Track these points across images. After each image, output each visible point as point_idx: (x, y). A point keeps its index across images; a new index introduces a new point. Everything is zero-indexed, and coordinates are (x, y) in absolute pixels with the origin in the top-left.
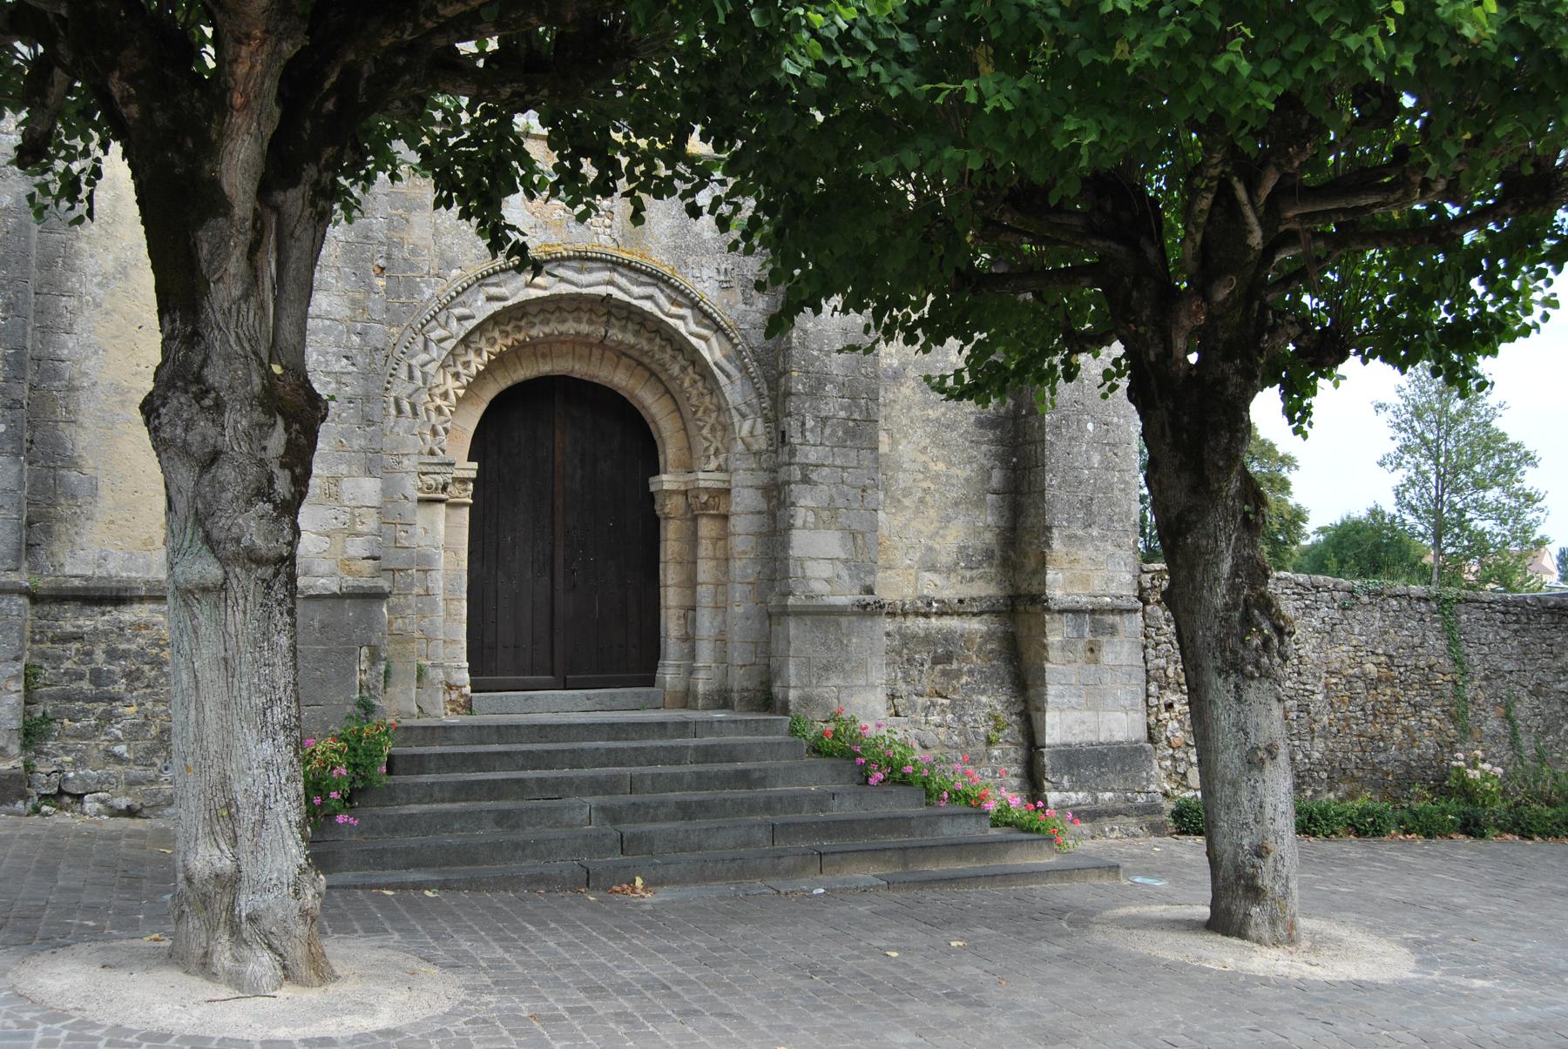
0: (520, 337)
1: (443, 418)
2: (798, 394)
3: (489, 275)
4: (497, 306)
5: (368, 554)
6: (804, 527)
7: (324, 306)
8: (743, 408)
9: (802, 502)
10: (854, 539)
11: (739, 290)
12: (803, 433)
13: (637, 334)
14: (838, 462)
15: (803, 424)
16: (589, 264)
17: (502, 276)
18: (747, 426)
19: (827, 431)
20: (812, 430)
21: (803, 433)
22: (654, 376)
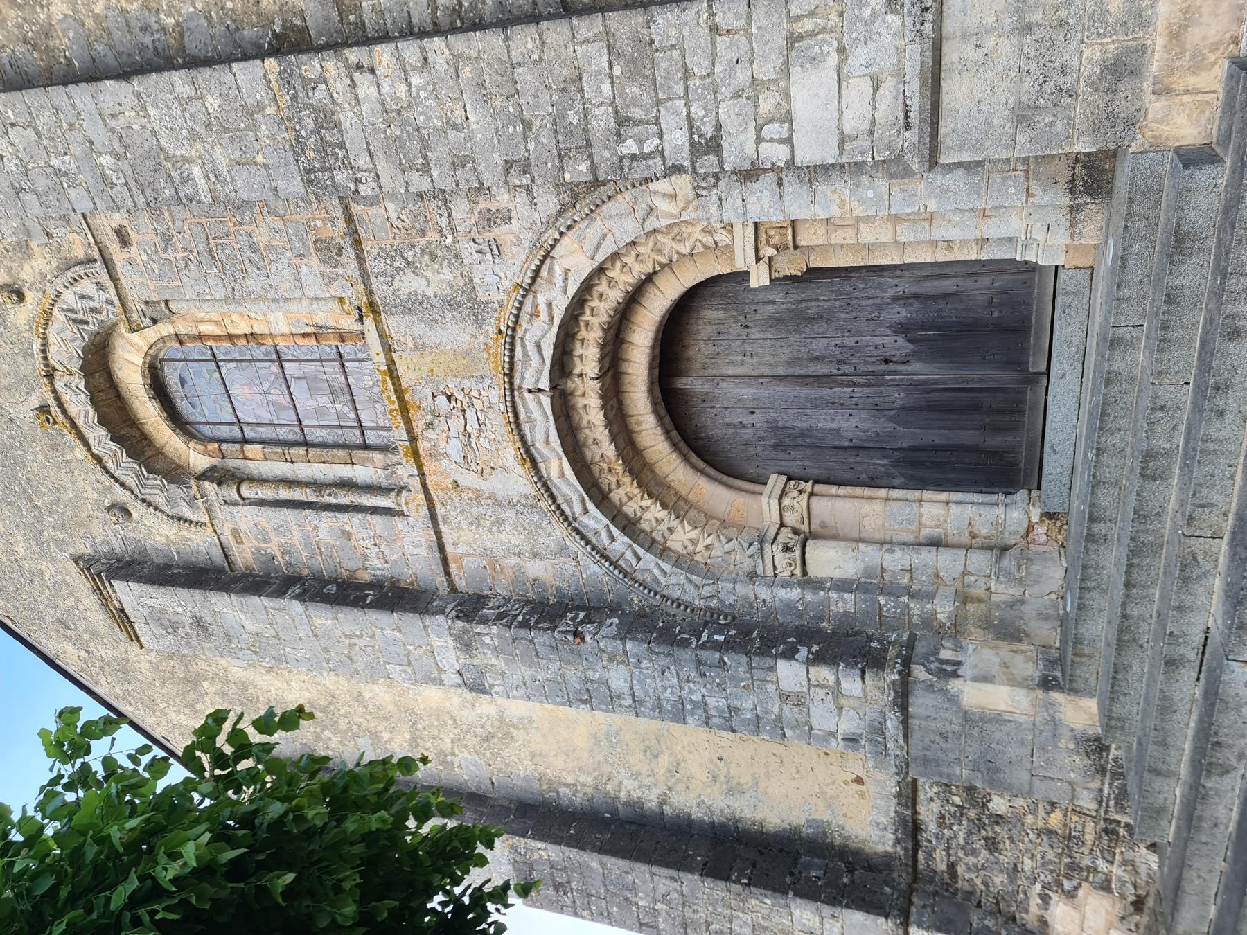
0: (620, 469)
1: (717, 544)
2: (593, 168)
3: (563, 513)
4: (591, 506)
5: (859, 680)
6: (789, 141)
7: (621, 683)
8: (640, 214)
9: (750, 149)
10: (800, 37)
11: (497, 231)
12: (646, 157)
13: (507, 662)
14: (679, 89)
15: (633, 157)
16: (522, 416)
17: (560, 500)
18: (663, 205)
19: (637, 114)
20: (640, 142)
21: (646, 157)
22: (634, 298)
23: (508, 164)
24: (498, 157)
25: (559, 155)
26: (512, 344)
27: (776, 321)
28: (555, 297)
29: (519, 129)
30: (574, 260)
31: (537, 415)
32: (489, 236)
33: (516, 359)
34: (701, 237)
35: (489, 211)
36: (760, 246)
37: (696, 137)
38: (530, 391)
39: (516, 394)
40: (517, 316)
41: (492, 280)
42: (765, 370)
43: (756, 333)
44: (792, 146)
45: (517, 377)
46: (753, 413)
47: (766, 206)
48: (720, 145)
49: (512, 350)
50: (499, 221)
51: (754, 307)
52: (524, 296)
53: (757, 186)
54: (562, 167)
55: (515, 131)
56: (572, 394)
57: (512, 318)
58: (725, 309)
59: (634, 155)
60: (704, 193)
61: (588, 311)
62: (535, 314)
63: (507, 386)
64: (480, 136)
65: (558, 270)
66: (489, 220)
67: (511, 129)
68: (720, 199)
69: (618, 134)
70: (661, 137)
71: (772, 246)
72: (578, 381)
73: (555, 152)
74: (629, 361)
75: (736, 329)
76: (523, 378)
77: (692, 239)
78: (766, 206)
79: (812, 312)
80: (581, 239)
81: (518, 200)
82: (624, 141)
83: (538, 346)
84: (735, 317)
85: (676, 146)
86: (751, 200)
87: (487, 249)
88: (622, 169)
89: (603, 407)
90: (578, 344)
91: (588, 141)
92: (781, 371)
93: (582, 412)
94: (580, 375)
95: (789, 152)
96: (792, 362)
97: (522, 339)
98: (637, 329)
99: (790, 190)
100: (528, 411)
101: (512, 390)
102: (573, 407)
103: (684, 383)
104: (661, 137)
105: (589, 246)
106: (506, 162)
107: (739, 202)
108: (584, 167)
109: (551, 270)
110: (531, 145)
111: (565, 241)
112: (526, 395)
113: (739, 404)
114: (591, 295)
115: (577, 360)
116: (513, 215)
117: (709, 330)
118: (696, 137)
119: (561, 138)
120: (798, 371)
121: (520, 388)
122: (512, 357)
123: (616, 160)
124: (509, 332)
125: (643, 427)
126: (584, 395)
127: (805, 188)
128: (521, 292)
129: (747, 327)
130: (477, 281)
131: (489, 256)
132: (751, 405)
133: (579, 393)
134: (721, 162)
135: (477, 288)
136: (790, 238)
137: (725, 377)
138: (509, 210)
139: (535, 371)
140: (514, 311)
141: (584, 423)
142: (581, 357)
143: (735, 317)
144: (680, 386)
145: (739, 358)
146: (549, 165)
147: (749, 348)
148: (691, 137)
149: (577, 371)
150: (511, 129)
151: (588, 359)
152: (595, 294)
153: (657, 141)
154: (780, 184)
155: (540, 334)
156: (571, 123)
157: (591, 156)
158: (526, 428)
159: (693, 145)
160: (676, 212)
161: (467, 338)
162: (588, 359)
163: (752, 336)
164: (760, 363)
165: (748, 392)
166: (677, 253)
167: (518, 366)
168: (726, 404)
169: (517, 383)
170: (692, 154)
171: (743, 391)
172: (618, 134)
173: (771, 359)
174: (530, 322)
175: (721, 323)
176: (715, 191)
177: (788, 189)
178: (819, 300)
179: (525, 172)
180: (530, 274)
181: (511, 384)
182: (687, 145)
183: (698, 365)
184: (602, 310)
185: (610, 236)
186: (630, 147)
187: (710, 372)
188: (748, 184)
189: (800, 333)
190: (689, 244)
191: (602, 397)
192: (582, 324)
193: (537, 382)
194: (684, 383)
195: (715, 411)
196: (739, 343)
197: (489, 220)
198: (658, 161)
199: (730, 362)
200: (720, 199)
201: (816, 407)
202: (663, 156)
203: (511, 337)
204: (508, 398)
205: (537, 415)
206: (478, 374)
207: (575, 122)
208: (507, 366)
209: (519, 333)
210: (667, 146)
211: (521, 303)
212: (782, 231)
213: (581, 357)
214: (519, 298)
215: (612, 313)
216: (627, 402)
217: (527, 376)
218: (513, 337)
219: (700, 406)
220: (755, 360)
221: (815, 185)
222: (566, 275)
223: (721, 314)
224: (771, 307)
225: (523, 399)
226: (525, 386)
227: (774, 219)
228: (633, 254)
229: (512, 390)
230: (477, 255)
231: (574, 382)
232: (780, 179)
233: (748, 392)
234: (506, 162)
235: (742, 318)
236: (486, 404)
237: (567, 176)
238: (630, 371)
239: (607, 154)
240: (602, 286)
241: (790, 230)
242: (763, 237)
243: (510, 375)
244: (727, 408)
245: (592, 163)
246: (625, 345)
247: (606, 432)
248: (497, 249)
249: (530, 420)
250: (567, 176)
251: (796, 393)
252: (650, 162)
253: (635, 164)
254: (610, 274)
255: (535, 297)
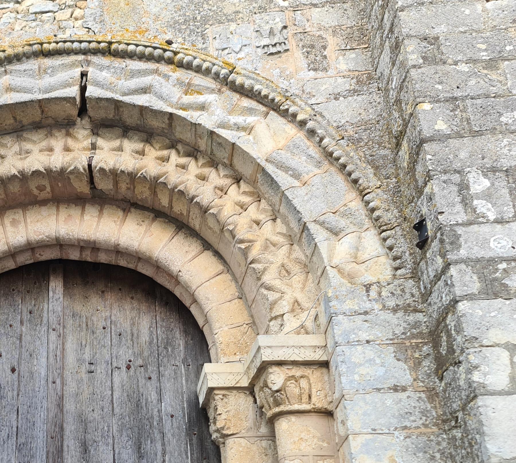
8: (331, 218)
12: (466, 202)
15: (463, 187)
16: (48, 62)
21: (466, 202)
23: (434, 41)
24: (441, 30)
25: (456, 99)
26: (150, 58)
27: (137, 404)
28: (216, 113)
29: (484, 56)
30: (265, 139)
31: (48, 81)
32: (292, 44)
33: (128, 61)
34: (288, 298)
35: (324, 48)
36: (284, 368)
37: (504, 265)
38: (84, 75)
39: (81, 57)
40: (188, 66)
41: (236, 43)
42: (71, 387)
43: (120, 378)
44: (508, 393)
45: (105, 61)
46: (13, 370)
47: (363, 370)
48: (496, 296)
49: (142, 57)
50: (312, 57)
51: (154, 376)
52: (217, 75)
53: (390, 359)
54: (438, 101)
55: (480, 50)
56: (68, 134)
57: (187, 59)
58: (151, 343)
59: (468, 187)
60: (373, 294)
61: (183, 160)
62: (189, 89)
63: (93, 45)
64: (467, 12)
65: (251, 119)
66: (312, 47)
67: (483, 47)
68: (366, 313)
69: (494, 170)
70: (497, 221)
71: (284, 384)
72: (87, 143)
73: (458, 93)
74: (101, 211)
75: (125, 354)
76: (102, 68)
77: (284, 288)
78: (363, 370)
79: (147, 446)
80: (292, 148)
81: (340, 80)
82: (485, 175)
83: (145, 90)
84: (141, 354)
85: (486, 241)
86: (369, 352)
87: (276, 40)
88: (445, 172)
89: (49, 171)
90: (139, 146)
91: (479, 133)
92: (70, 406)
93: (44, 144)
94: (94, 147)
95: (499, 388)
96: (83, 421)
97: (156, 71)
98: (142, 229)
99: (389, 402)
100: (54, 70)
101: (85, 52)
102: (50, 134)
103: (56, 287)
104: (497, 221)
105: (285, 157)
106: (437, 38)
107: (365, 336)
108: (441, 126)
109: (250, 111)
110: (464, 67)
111: (291, 130)
112: (77, 72)
113: (25, 355)
114: (204, 165)
115: (117, 143)
116: (320, 74)
117: (124, 323)
118: (503, 266)
119: (479, 101)
120: (70, 428)
121: (89, 63)
122: (131, 56)
123: (457, 165)
124: (168, 54)
125: (9, 229)
126: (67, 149)
127: (394, 421)
128: (224, 72)
129: (128, 367)
130: (233, 26)
131: (266, 41)
132: (24, 368)
133: (70, 142)
134: (470, 297)
135: (222, 26)
136: (296, 407)
137: (62, 337)
138: (325, 70)
139: (108, 81)
140: (196, 63)
141: (28, 146)
142: (120, 149)
143: (141, 354)
144: (52, 284)
145: (87, 357)
146: (440, 87)
147: (101, 369)
148: (503, 260)
149: (100, 142)
150: (483, 47)
151: (117, 155)
152: (206, 171)
153: (492, 217)
154: (395, 389)
155: (163, 92)
156: (501, 115)
157: (459, 136)
158: (32, 64)
159: (492, 261)
160: (336, 261)
161: (155, 10)
162: (117, 155)
163: (116, 373)
164: (80, 382)
165: (41, 366)
166: (265, 269)
167: (118, 63)
168: (26, 338)
169: (95, 59)
170: (478, 260)
171: (44, 360)
172: (494, 170)
173: (86, 394)
174: (180, 83)
175: (134, 337)
176: (377, 306)
177: (390, 399)
178: (164, 454)
179: (424, 58)
180: (247, 83)
181: (95, 52)
182: (489, 255)
183: (78, 307)
184: (184, 178)
185: (296, 183)
186: (479, 184)
187: (70, 322)
188: (392, 349)
189: (121, 431)
190: (277, 283)
191: (62, 171)
192: (165, 152)
193: (97, 84)
194: (56, 287)
195: (16, 324)
196: (108, 357)
197: (312, 47)
198: (462, 217)
199: (82, 347)
200: (366, 313)
201: (19, 449)
202: (470, 223)
203: (161, 57)
204: (76, 45)
205: (48, 81)
206: (107, 18)
207: (503, 119)
208: (122, 47)
209: (164, 68)
210: (485, 229)
211: (207, 72)
212: (305, 398)
213: (120, 149)
214: (215, 69)
215: (181, 187)
216: (44, 211)
217: (105, 74)
218: (159, 59)
219: (24, 308)
220: (84, 376)
221: (401, 435)
222: (244, 129)
223: (145, 337)
224: (154, 396)
225: (73, 65)
226: (91, 71)
227: (344, 379)
228: (261, 217)
229: (85, 52)
230: (267, 28)
231: (86, 137)
232: (404, 389)
233: (41, 366)
234: (437, 38)
235: (140, 362)
236: (64, 24)
237: (427, 106)
238: (87, 217)
239: (463, 155)
240: (217, 178)
241: (308, 407)
242: (297, 372)
243: (108, 51)
244: (21, 339)
245: (449, 137)
246: (121, 213)
247: (14, 171)
248: (275, 51)
249: (42, 72)
250: (427, 106)
251: (39, 424)
252: (459, 207)
253: (456, 189)
254: (233, 190)
255: (212, 91)
